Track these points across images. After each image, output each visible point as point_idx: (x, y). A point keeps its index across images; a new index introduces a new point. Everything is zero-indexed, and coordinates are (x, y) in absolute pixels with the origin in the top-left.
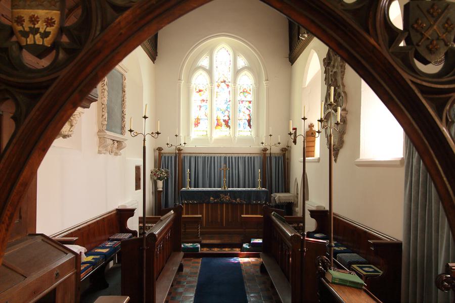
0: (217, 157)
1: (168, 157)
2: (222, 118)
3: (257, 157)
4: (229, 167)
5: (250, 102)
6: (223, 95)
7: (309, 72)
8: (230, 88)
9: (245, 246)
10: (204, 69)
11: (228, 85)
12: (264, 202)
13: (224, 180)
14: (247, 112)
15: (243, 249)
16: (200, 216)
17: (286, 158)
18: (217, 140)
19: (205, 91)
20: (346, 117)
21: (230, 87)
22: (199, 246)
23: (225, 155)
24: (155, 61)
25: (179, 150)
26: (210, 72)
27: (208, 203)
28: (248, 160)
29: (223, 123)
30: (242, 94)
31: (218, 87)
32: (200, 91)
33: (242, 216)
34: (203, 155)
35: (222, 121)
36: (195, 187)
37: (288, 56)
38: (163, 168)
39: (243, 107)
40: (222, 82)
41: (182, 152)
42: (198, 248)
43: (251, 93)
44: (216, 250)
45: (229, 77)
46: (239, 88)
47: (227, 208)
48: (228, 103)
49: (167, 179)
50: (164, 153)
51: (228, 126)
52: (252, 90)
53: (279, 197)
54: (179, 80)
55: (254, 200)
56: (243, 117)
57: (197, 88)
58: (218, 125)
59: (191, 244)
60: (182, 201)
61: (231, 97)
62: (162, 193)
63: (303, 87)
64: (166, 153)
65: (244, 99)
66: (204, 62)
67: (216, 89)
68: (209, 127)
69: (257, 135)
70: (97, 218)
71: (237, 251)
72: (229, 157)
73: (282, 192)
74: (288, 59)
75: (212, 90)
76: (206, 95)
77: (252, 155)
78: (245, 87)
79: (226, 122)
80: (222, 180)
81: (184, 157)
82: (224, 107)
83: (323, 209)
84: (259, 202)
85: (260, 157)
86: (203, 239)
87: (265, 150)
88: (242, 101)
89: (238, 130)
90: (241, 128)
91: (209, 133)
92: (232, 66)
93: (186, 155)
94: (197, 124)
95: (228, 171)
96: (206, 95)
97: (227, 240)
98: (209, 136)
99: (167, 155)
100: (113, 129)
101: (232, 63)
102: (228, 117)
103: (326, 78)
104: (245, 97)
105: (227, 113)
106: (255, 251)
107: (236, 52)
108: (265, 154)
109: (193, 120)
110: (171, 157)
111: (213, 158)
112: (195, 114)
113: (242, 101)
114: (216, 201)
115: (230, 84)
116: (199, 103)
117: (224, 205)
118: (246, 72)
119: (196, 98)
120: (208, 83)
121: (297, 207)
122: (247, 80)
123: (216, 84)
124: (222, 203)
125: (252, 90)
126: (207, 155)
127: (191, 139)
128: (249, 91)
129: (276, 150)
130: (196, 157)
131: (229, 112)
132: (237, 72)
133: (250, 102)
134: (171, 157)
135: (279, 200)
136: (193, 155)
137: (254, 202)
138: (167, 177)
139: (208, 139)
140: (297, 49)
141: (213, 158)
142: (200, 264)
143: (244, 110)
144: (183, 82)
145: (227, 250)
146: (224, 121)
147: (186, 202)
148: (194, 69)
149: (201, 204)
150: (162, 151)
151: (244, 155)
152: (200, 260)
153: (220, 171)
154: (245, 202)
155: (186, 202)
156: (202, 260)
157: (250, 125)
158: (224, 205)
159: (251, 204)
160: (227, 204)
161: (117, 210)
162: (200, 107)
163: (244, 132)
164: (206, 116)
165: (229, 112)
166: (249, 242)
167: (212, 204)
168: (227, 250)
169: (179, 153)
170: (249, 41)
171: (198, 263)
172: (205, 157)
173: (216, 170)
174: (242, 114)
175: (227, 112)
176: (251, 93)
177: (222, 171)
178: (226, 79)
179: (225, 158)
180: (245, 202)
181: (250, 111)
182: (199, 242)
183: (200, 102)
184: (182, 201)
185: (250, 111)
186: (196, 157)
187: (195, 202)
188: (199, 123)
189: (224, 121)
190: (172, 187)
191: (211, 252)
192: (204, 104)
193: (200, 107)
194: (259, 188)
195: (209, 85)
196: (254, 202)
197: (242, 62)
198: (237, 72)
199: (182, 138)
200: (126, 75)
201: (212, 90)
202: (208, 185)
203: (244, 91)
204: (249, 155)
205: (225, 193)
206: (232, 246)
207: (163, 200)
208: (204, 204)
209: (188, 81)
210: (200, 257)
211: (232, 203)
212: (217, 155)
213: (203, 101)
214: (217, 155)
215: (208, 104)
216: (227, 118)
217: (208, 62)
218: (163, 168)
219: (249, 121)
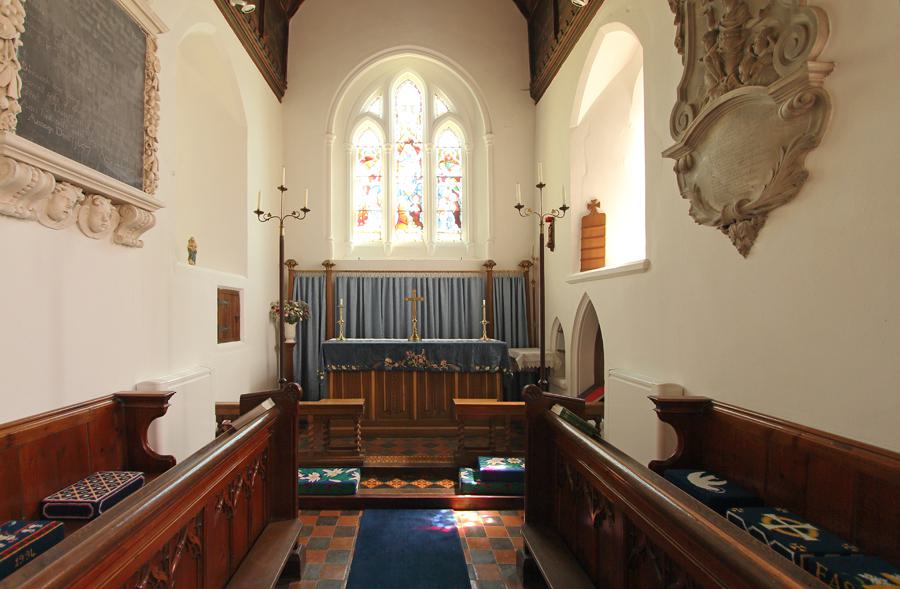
0: (400, 279)
1: (307, 279)
2: (408, 207)
3: (476, 278)
4: (422, 295)
5: (458, 179)
6: (409, 167)
7: (593, 69)
8: (421, 155)
9: (466, 476)
10: (375, 117)
11: (417, 149)
12: (497, 368)
13: (414, 324)
14: (453, 198)
15: (461, 488)
16: (361, 401)
17: (530, 280)
18: (399, 249)
19: (375, 158)
20: (821, 88)
21: (421, 153)
22: (357, 476)
23: (413, 275)
24: (283, 99)
25: (328, 264)
26: (384, 123)
27: (380, 370)
28: (459, 284)
29: (410, 218)
30: (442, 165)
31: (400, 151)
32: (368, 159)
33: (457, 402)
34: (373, 275)
35: (407, 214)
36: (358, 337)
37: (528, 87)
38: (297, 301)
39: (445, 189)
40: (406, 143)
41: (333, 268)
42: (353, 485)
43: (460, 162)
44: (397, 488)
45: (419, 133)
46: (438, 152)
47: (420, 381)
48: (418, 182)
49: (305, 322)
50: (300, 271)
51: (417, 222)
52: (460, 157)
53: (525, 356)
54: (328, 133)
55: (476, 364)
56: (446, 206)
57: (362, 153)
58: (400, 221)
59: (339, 471)
60: (325, 364)
61: (422, 171)
62: (295, 348)
63: (571, 127)
64: (303, 272)
65: (446, 173)
66: (374, 105)
67: (396, 156)
68: (383, 224)
69: (473, 239)
70: (103, 400)
71: (446, 488)
72: (422, 279)
73: (525, 347)
74: (529, 92)
75: (388, 155)
76: (378, 167)
77: (466, 276)
78: (449, 151)
79: (416, 217)
80: (409, 322)
81: (338, 279)
82: (411, 190)
83: (678, 396)
84: (488, 368)
85: (481, 280)
86: (369, 453)
87: (490, 264)
88: (444, 178)
89: (438, 230)
90: (443, 228)
91: (384, 236)
92: (424, 114)
93: (340, 275)
94: (362, 220)
95: (419, 302)
96: (378, 167)
97: (422, 460)
98: (384, 240)
99: (304, 275)
100: (108, 166)
101: (424, 109)
102: (420, 206)
103: (681, 35)
104: (449, 170)
105: (416, 201)
106: (494, 493)
107: (431, 85)
108: (490, 273)
109: (355, 213)
110: (313, 279)
111: (391, 281)
112: (358, 200)
113: (444, 178)
114: (396, 365)
115: (420, 146)
116: (366, 181)
117: (415, 374)
118: (450, 123)
119: (359, 172)
120: (382, 143)
121: (564, 377)
122: (451, 139)
123: (397, 146)
124: (410, 370)
125: (460, 157)
126: (380, 275)
127: (353, 246)
128: (455, 159)
129: (507, 262)
130: (359, 279)
131: (420, 197)
132: (433, 123)
133: (458, 179)
134: (313, 279)
135: (524, 363)
136: (354, 275)
137: (478, 368)
138: (303, 317)
139: (382, 247)
140: (544, 72)
141: (391, 281)
142: (355, 538)
143: (446, 193)
144: (335, 138)
145: (422, 488)
146: (412, 214)
147: (334, 368)
148: (354, 117)
149: (367, 372)
150: (296, 268)
151: (451, 276)
152: (354, 521)
153: (406, 302)
154: (458, 369)
155: (334, 368)
156: (361, 519)
157: (458, 222)
158: (415, 374)
159: (471, 373)
160: (420, 372)
161: (117, 397)
162: (369, 188)
163: (449, 234)
164: (379, 205)
165: (420, 197)
166: (475, 465)
167: (389, 371)
168: (422, 488)
169: (327, 272)
170: (454, 59)
171: (348, 532)
172: (377, 279)
173: (398, 300)
174: (443, 201)
175: (416, 199)
176: (460, 162)
177: (410, 303)
178: (413, 138)
179: (415, 280)
180: (458, 369)
181: (458, 195)
182: (358, 465)
183: (367, 179)
184: (325, 364)
185: (458, 195)
186: (359, 279)
187: (354, 368)
188: (366, 218)
189: (412, 214)
190: (314, 334)
191: (383, 493)
192: (375, 182)
193: (369, 188)
194: (484, 339)
195: (384, 146)
196: (478, 368)
197: (442, 106)
198: (433, 123)
199: (333, 243)
200: (161, 40)
201: (388, 155)
202: (382, 333)
203: (446, 159)
204: (459, 275)
205: (416, 348)
206: (434, 474)
207: (298, 362)
208: (373, 373)
209: (346, 140)
210: (360, 509)
211: (431, 372)
212: (400, 275)
213: (374, 177)
214: (400, 275)
215: (382, 184)
216: (417, 210)
217: (381, 107)
218: (297, 301)
219: (457, 214)
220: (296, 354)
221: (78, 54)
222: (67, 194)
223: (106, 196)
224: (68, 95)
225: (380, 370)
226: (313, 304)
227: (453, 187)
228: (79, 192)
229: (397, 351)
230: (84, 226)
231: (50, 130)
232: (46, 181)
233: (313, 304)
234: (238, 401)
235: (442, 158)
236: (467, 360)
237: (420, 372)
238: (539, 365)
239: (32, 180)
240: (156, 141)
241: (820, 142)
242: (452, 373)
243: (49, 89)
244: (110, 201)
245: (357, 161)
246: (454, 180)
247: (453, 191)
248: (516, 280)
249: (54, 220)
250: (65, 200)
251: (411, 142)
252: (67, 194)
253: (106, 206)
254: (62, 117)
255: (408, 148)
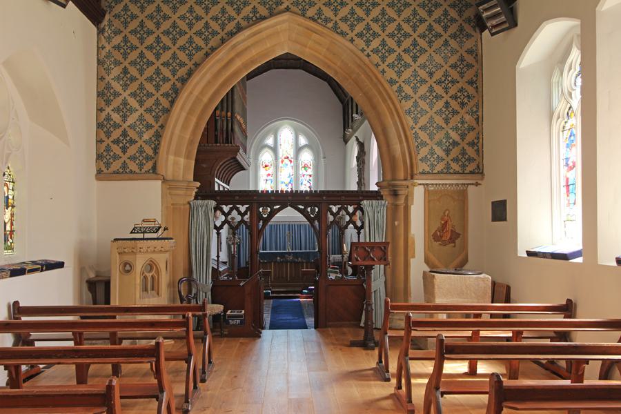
8: (292, 164)
11: (291, 161)
14: (308, 185)
26: (275, 150)
32: (266, 166)
43: (311, 167)
45: (291, 154)
66: (270, 141)
67: (281, 165)
76: (271, 170)
78: (306, 162)
82: (287, 182)
87: (16, 303)
88: (304, 175)
113: (304, 175)
115: (292, 160)
116: (265, 177)
122: (307, 157)
123: (280, 160)
124: (287, 262)
133: (310, 176)
149: (270, 263)
160: (291, 263)
162: (267, 180)
192: (269, 178)
193: (267, 180)
197: (303, 141)
198: (298, 150)
208: (273, 264)
209: (256, 158)
211: (294, 262)
220: (236, 260)
225: (275, 262)
226: (243, 236)
227: (308, 179)
229: (282, 255)
233: (243, 236)
234: (7, 371)
235: (264, 166)
236: (308, 258)
237: (291, 263)
238: (357, 241)
241: (327, 344)
242: (303, 263)
245: (261, 167)
246: (308, 176)
251: (288, 158)
255: (286, 161)
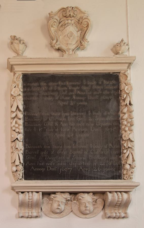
221: (59, 122)
222: (57, 199)
223: (88, 193)
224: (54, 147)
228: (68, 196)
230: (78, 213)
231: (43, 170)
232: (36, 197)
239: (29, 199)
240: (132, 141)
243: (42, 150)
244: (92, 194)
247: (88, 12)
248: (22, 205)
249: (86, 215)
250: (57, 202)
252: (57, 199)
253: (88, 198)
254: (51, 160)
